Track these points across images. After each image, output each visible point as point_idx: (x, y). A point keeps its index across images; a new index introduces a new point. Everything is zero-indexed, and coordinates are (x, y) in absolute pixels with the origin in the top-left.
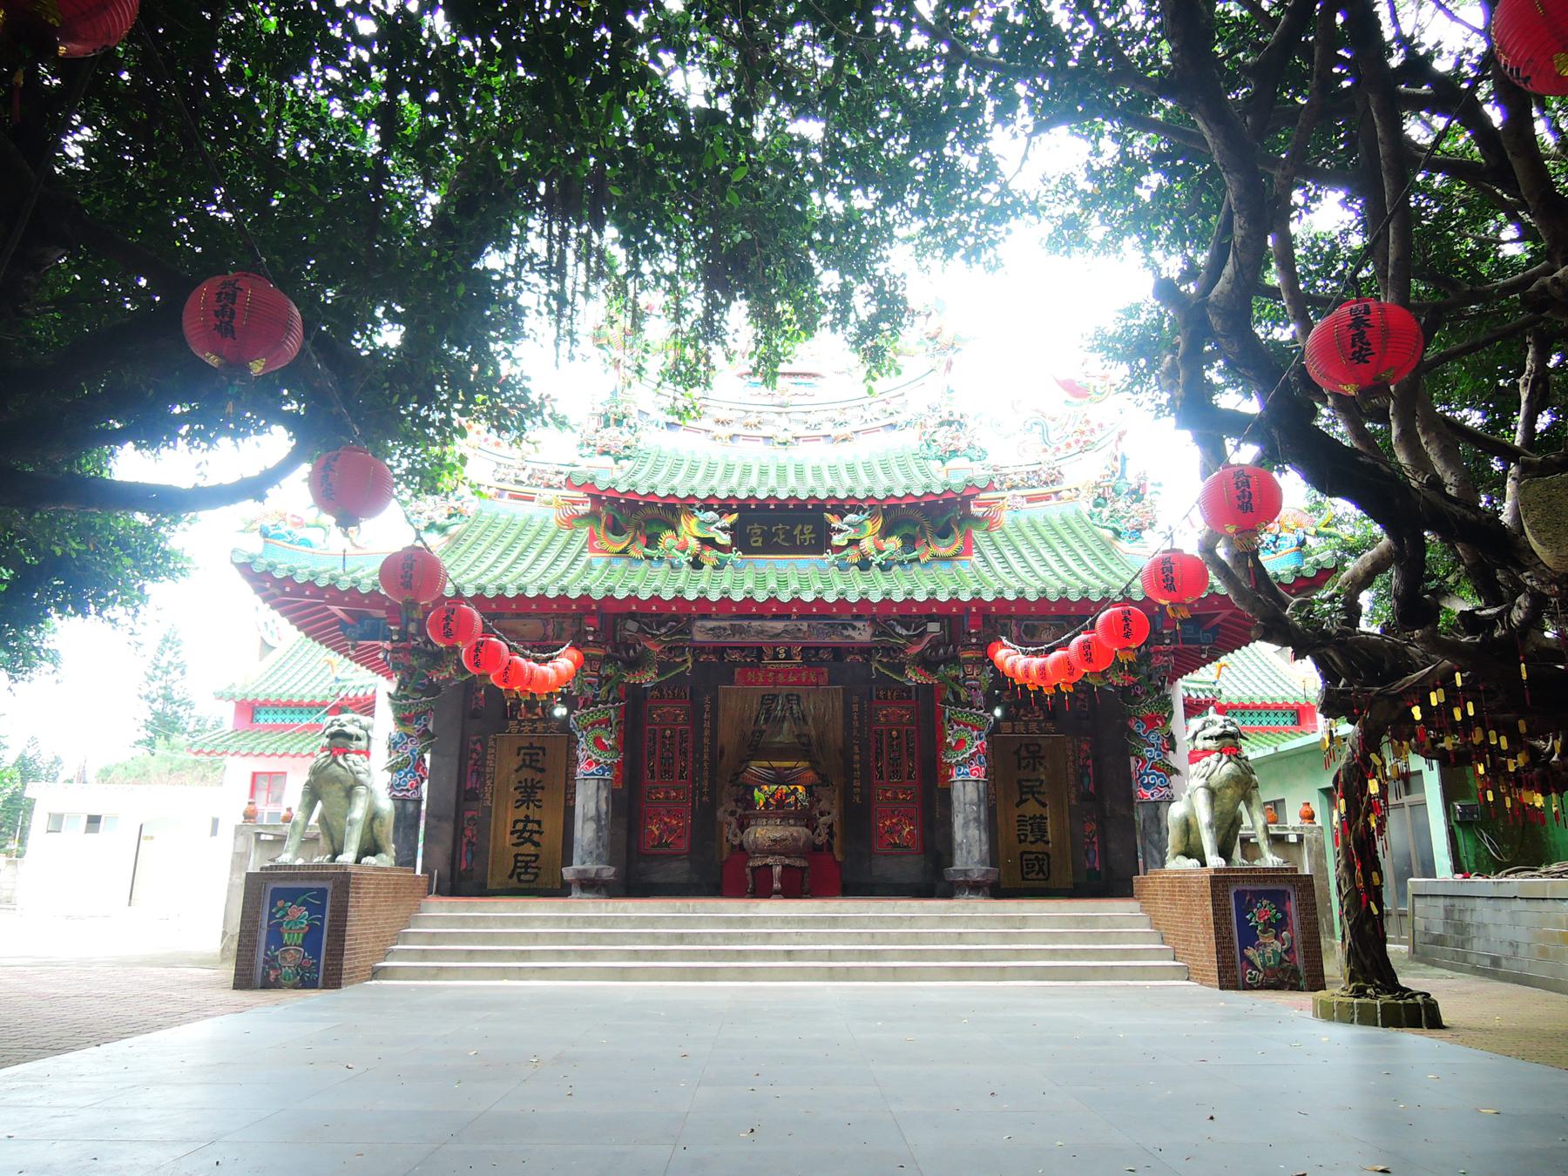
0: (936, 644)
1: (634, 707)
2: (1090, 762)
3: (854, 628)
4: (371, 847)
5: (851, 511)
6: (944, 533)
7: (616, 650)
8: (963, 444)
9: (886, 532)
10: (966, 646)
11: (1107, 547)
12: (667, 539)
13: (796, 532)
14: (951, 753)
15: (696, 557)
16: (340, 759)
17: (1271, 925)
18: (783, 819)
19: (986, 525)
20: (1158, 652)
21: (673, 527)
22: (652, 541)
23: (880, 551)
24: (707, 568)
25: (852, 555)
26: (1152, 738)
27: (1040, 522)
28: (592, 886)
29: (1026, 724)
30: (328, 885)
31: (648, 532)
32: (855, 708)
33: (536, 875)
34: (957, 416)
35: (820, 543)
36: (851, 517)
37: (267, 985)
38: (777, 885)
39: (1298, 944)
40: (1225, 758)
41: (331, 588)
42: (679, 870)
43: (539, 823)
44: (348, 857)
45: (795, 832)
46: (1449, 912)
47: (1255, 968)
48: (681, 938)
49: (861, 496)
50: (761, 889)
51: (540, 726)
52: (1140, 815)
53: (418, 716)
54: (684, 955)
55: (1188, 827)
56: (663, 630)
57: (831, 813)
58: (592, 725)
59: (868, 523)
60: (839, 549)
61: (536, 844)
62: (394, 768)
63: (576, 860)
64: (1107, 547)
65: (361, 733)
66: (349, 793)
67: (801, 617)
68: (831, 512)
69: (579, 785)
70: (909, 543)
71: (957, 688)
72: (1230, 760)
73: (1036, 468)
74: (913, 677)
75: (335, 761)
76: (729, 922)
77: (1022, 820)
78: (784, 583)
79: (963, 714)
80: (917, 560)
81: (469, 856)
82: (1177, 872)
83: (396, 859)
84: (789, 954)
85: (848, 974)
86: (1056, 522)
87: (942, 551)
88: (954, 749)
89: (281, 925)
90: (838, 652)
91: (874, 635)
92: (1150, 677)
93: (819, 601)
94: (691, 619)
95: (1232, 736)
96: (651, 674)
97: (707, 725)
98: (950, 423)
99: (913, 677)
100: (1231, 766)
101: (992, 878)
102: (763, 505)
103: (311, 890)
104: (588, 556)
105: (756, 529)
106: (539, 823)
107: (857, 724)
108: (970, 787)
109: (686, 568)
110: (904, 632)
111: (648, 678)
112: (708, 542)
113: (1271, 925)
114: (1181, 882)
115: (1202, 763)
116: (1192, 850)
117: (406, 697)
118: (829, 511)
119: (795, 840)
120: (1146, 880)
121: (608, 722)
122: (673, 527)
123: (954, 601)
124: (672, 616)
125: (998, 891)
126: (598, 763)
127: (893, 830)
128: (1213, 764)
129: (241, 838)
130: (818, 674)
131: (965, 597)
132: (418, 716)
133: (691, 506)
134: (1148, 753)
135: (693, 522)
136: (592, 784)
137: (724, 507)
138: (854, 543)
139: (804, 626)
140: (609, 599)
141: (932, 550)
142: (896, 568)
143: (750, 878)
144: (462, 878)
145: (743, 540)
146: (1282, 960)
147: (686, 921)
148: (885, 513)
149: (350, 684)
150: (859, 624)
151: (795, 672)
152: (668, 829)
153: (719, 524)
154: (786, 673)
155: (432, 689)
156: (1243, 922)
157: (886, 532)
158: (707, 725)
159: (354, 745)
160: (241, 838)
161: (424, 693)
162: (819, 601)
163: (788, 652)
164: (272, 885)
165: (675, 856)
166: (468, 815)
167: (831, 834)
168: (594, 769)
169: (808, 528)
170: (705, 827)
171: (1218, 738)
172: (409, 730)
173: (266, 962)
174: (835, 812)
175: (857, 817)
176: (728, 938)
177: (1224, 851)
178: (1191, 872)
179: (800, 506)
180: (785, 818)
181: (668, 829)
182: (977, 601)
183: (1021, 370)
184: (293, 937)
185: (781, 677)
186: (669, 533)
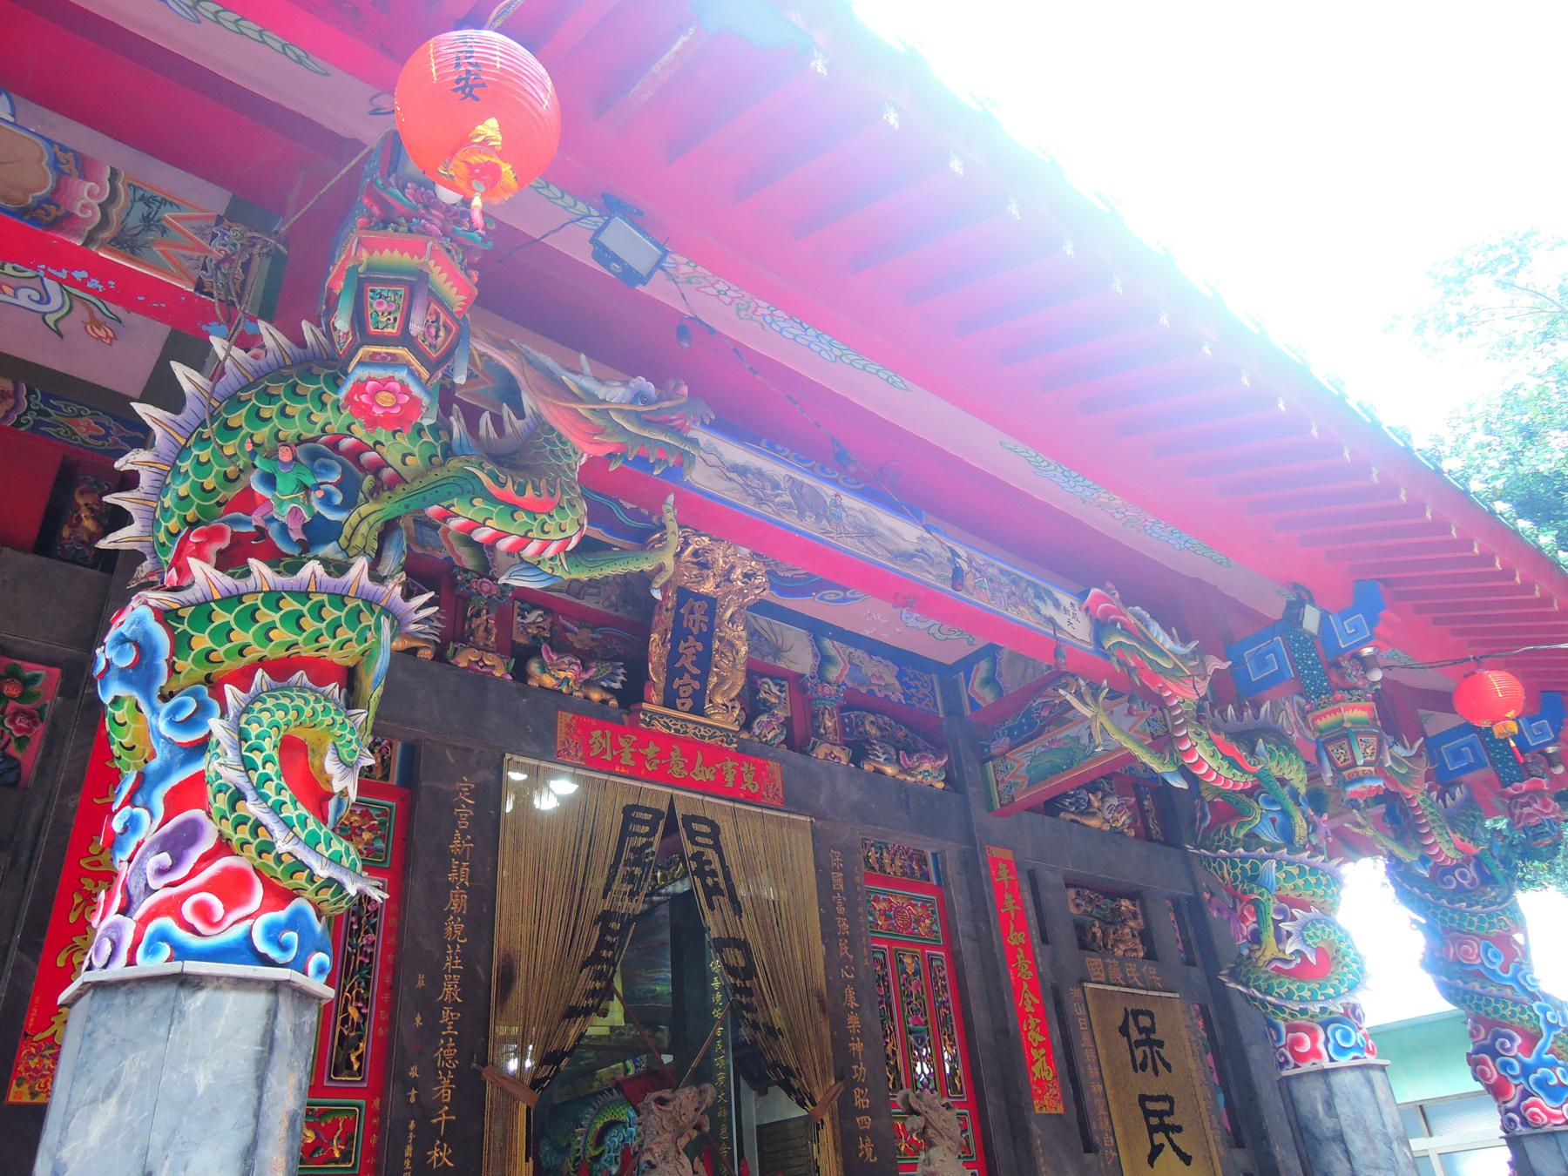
58: (281, 670)
107: (844, 926)
158: (459, 874)
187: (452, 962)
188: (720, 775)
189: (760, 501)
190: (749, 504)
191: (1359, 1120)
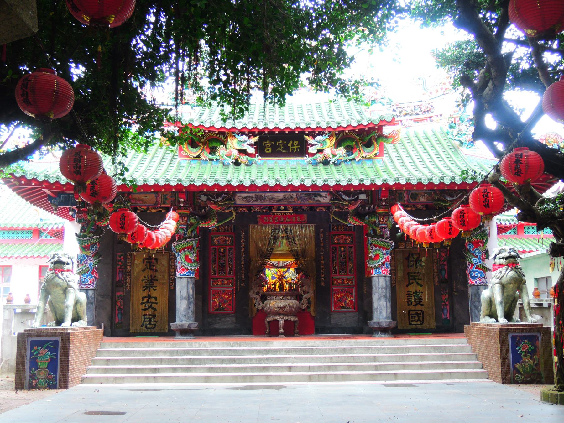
0: (364, 204)
2: (445, 263)
3: (321, 196)
4: (76, 318)
6: (369, 144)
7: (195, 210)
8: (378, 97)
9: (338, 144)
10: (380, 206)
11: (455, 150)
12: (221, 150)
13: (290, 145)
14: (371, 262)
15: (236, 160)
16: (60, 274)
17: (529, 352)
18: (284, 296)
19: (391, 140)
21: (224, 144)
22: (213, 150)
23: (334, 156)
24: (243, 166)
26: (477, 253)
27: (421, 135)
28: (186, 332)
30: (59, 339)
31: (210, 146)
32: (322, 235)
33: (155, 325)
34: (375, 81)
35: (303, 151)
36: (319, 138)
37: (32, 387)
38: (281, 330)
39: (542, 361)
40: (510, 269)
41: (46, 181)
42: (229, 322)
43: (155, 298)
44: (67, 324)
47: (520, 373)
48: (233, 361)
50: (273, 331)
52: (470, 291)
53: (92, 245)
55: (491, 302)
56: (219, 199)
58: (184, 249)
59: (328, 141)
60: (312, 155)
62: (80, 273)
63: (177, 319)
64: (455, 150)
65: (69, 261)
66: (65, 291)
67: (293, 191)
68: (308, 135)
69: (178, 281)
70: (350, 150)
71: (375, 228)
72: (512, 270)
73: (419, 104)
74: (352, 222)
75: (57, 276)
76: (259, 352)
77: (409, 295)
78: (284, 174)
79: (378, 242)
80: (354, 159)
81: (120, 316)
82: (485, 325)
83: (88, 323)
84: (290, 369)
85: (319, 378)
86: (430, 134)
88: (373, 259)
89: (36, 358)
91: (331, 200)
93: (302, 186)
94: (234, 193)
95: (514, 257)
96: (214, 222)
97: (243, 245)
98: (372, 84)
99: (352, 222)
100: (512, 272)
101: (393, 325)
102: (271, 132)
103: (50, 341)
104: (178, 159)
106: (155, 298)
108: (382, 280)
109: (232, 166)
110: (347, 198)
111: (212, 224)
112: (243, 152)
113: (529, 352)
114: (486, 331)
115: (498, 271)
116: (492, 315)
117: (86, 236)
118: (307, 135)
119: (290, 307)
120: (472, 327)
122: (224, 144)
123: (373, 185)
124: (227, 193)
126: (187, 269)
127: (342, 300)
128: (504, 271)
129: (7, 312)
132: (92, 245)
133: (233, 133)
134: (475, 260)
135: (235, 141)
136: (185, 281)
137: (251, 133)
138: (320, 151)
139: (294, 195)
140: (192, 186)
141: (362, 154)
142: (343, 164)
143: (267, 326)
145: (261, 150)
146: (533, 369)
148: (337, 135)
149: (48, 222)
150: (323, 194)
152: (223, 301)
153: (248, 142)
154: (285, 217)
155: (98, 231)
156: (514, 351)
157: (338, 144)
158: (243, 245)
159: (66, 267)
160: (7, 312)
161: (95, 233)
162: (302, 186)
164: (30, 339)
165: (227, 315)
167: (309, 303)
168: (185, 272)
169: (296, 143)
171: (506, 258)
172: (88, 253)
173: (30, 376)
174: (311, 292)
175: (323, 294)
176: (260, 360)
177: (508, 315)
178: (491, 325)
179: (292, 132)
180: (285, 296)
181: (223, 301)
182: (385, 185)
183: (405, 97)
184: (43, 364)
185: (282, 219)
187: (243, 259)
188: (292, 220)
189: (249, 202)
190: (247, 203)
191: (376, 284)
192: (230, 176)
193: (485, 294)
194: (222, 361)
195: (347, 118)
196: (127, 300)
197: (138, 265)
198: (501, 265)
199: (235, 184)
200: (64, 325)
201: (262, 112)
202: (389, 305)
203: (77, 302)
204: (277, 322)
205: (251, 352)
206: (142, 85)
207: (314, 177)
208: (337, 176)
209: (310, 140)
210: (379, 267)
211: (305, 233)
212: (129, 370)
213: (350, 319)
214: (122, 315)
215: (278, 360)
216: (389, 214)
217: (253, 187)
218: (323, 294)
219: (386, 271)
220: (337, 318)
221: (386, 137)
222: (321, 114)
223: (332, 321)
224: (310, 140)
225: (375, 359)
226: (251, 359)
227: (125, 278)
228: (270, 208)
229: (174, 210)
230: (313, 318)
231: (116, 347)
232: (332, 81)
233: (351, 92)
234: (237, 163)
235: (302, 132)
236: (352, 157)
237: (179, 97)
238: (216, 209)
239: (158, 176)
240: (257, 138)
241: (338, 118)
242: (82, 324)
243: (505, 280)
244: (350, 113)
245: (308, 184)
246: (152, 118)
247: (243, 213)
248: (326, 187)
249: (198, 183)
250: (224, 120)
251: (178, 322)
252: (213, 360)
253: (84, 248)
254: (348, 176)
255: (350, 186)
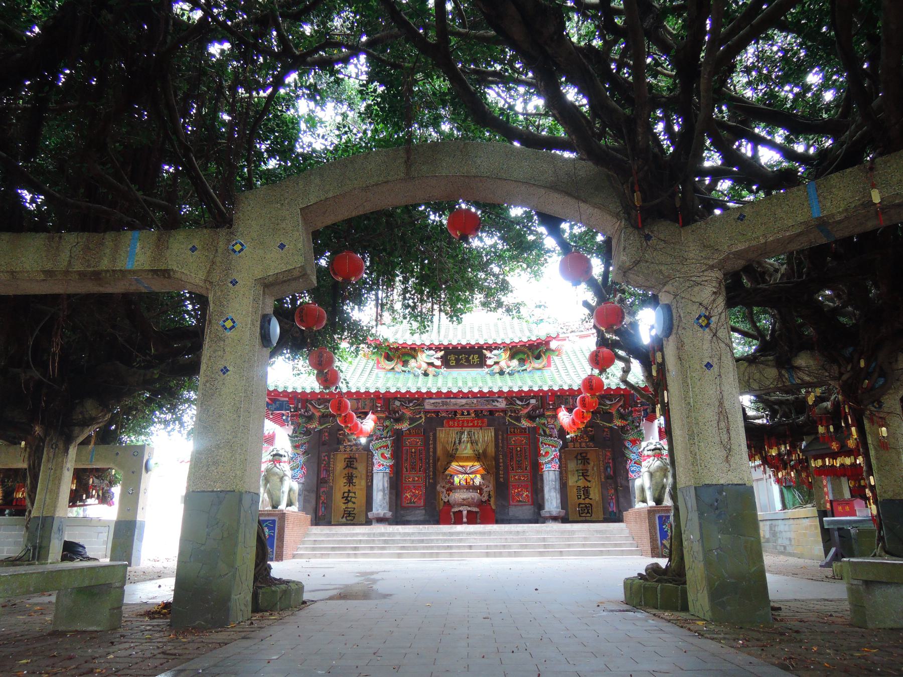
0: (535, 408)
1: (398, 438)
4: (290, 504)
5: (495, 349)
6: (538, 357)
8: (544, 317)
9: (512, 357)
12: (412, 363)
13: (471, 358)
15: (425, 371)
20: (635, 410)
21: (414, 357)
22: (405, 363)
23: (509, 367)
24: (431, 376)
25: (496, 368)
28: (381, 520)
29: (580, 443)
30: (276, 518)
31: (404, 359)
32: (500, 437)
35: (482, 363)
36: (495, 352)
38: (465, 520)
42: (420, 514)
45: (474, 495)
46: (771, 527)
48: (422, 541)
49: (499, 342)
50: (458, 520)
51: (354, 448)
53: (302, 445)
54: (424, 548)
55: (642, 490)
57: (490, 488)
59: (503, 354)
60: (490, 366)
61: (354, 503)
66: (282, 479)
69: (374, 475)
70: (522, 361)
74: (525, 423)
76: (444, 534)
78: (465, 383)
79: (548, 440)
84: (470, 547)
87: (537, 366)
90: (491, 412)
92: (633, 422)
94: (424, 399)
95: (659, 449)
97: (431, 446)
98: (540, 307)
99: (525, 423)
100: (659, 462)
102: (455, 347)
104: (376, 371)
105: (452, 357)
108: (551, 473)
109: (421, 377)
111: (405, 426)
112: (431, 364)
114: (639, 512)
116: (644, 501)
120: (628, 515)
121: (387, 446)
122: (414, 357)
123: (541, 391)
124: (416, 399)
125: (565, 520)
130: (482, 423)
131: (546, 388)
132: (302, 445)
134: (632, 456)
135: (424, 355)
136: (381, 475)
137: (438, 349)
138: (496, 363)
139: (475, 401)
140: (388, 392)
141: (532, 365)
142: (516, 374)
144: (320, 519)
147: (424, 534)
148: (510, 349)
150: (500, 400)
151: (472, 421)
152: (414, 495)
154: (468, 421)
155: (307, 432)
156: (661, 529)
157: (512, 357)
158: (431, 446)
159: (283, 459)
163: (468, 412)
166: (322, 490)
168: (381, 468)
170: (431, 494)
176: (445, 541)
179: (472, 347)
182: (551, 390)
186: (413, 360)
192: (420, 384)
193: (638, 483)
194: (413, 541)
195: (519, 335)
196: (329, 495)
197: (339, 465)
198: (649, 456)
199: (424, 390)
200: (280, 508)
201: (446, 330)
202: (558, 496)
203: (290, 490)
204: (461, 512)
205: (438, 534)
206: (352, 309)
207: (490, 384)
208: (510, 384)
209: (488, 354)
210: (549, 462)
211: (485, 437)
212: (333, 549)
213: (528, 510)
214: (325, 508)
215: (461, 540)
216: (555, 417)
217: (439, 394)
218: (502, 488)
219: (556, 465)
220: (513, 511)
221: (553, 351)
222: (497, 331)
223: (511, 514)
224: (488, 354)
225: (544, 539)
226: (437, 540)
227: (329, 476)
228: (455, 413)
229: (373, 413)
230: (493, 511)
231: (321, 532)
232: (500, 304)
233: (514, 312)
234: (426, 374)
235: (481, 347)
236: (524, 368)
237: (378, 319)
238: (408, 414)
239: (359, 385)
240: (443, 352)
241: (511, 335)
242: (295, 508)
243: (652, 468)
244: (522, 331)
245: (486, 390)
246: (358, 335)
247: (431, 418)
248: (501, 392)
249: (393, 390)
250: (412, 334)
251: (374, 511)
252: (405, 540)
253: (296, 447)
254: (520, 384)
255: (521, 391)
